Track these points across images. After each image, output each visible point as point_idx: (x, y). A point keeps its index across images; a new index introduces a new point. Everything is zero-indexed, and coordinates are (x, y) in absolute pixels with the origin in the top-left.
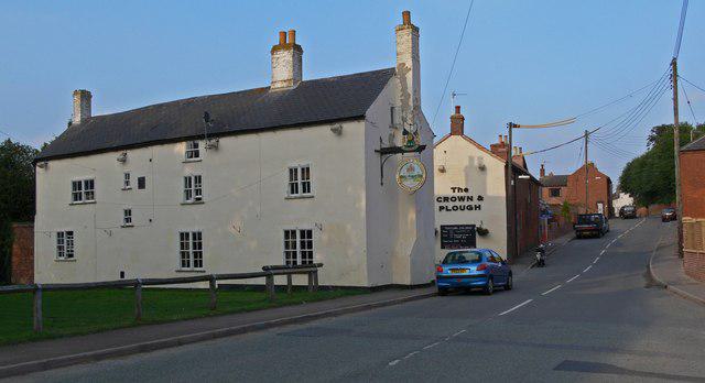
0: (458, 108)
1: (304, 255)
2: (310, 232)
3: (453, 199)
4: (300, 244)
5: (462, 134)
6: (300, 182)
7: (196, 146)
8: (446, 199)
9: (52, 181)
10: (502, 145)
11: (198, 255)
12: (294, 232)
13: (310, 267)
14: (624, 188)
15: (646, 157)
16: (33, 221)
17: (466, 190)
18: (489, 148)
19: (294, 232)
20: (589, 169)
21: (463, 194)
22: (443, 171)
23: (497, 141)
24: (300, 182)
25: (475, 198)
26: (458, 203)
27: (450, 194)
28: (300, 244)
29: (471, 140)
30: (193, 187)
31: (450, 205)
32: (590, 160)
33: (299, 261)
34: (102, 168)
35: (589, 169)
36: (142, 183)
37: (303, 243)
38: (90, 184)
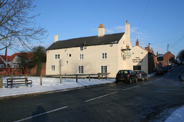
0: (137, 40)
1: (105, 71)
2: (106, 66)
3: (136, 60)
4: (104, 68)
5: (138, 46)
6: (105, 55)
7: (82, 48)
8: (134, 60)
9: (51, 55)
10: (147, 47)
11: (82, 71)
12: (103, 66)
13: (107, 74)
14: (149, 73)
15: (4, 56)
16: (46, 62)
17: (139, 58)
18: (144, 49)
19: (103, 66)
20: (169, 53)
21: (134, 61)
22: (133, 54)
23: (146, 47)
24: (105, 55)
25: (141, 60)
26: (137, 61)
27: (135, 59)
28: (104, 68)
29: (140, 47)
30: (82, 56)
31: (135, 61)
32: (169, 51)
33: (104, 72)
34: (61, 52)
35: (169, 53)
36: (70, 55)
37: (105, 69)
38: (59, 55)
